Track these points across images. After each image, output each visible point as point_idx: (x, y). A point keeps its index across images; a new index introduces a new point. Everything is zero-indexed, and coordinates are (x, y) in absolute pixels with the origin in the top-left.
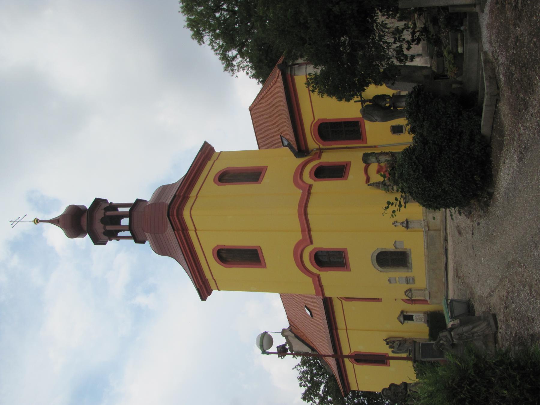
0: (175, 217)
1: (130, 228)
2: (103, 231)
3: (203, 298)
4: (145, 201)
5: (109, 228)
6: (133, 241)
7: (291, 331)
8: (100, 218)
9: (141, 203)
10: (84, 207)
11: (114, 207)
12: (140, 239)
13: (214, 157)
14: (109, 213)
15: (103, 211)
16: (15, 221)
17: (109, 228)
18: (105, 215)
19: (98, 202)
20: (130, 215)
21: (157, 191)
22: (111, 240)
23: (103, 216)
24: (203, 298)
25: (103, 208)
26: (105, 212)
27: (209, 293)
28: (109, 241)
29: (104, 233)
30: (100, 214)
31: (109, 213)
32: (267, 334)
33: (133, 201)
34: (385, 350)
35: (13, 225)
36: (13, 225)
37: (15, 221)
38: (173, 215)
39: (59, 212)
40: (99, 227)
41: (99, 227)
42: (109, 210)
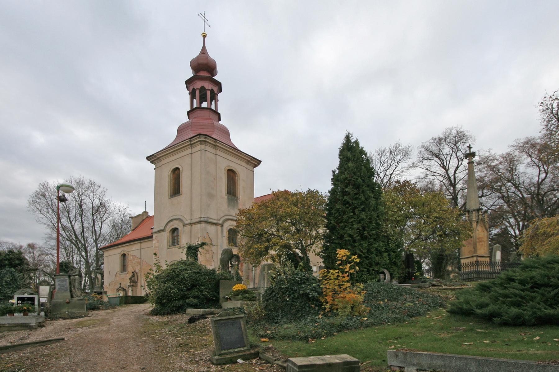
0: (199, 139)
1: (200, 108)
2: (195, 88)
3: (148, 158)
4: (220, 120)
5: (197, 93)
6: (189, 110)
7: (147, 217)
8: (204, 86)
9: (217, 117)
10: (216, 74)
11: (214, 97)
12: (190, 116)
13: (249, 167)
14: (209, 93)
15: (210, 89)
16: (204, 17)
17: (197, 93)
18: (207, 89)
19: (219, 85)
20: (209, 109)
21: (226, 130)
22: (189, 94)
23: (206, 88)
24: (148, 158)
25: (213, 89)
26: (209, 89)
27: (152, 162)
28: (189, 92)
29: (194, 89)
30: (208, 86)
31: (209, 93)
32: (73, 190)
33: (219, 111)
34: (130, 269)
35: (200, 15)
36: (200, 15)
37: (204, 17)
38: (200, 138)
39: (212, 54)
40: (198, 85)
41: (198, 85)
42: (211, 93)
